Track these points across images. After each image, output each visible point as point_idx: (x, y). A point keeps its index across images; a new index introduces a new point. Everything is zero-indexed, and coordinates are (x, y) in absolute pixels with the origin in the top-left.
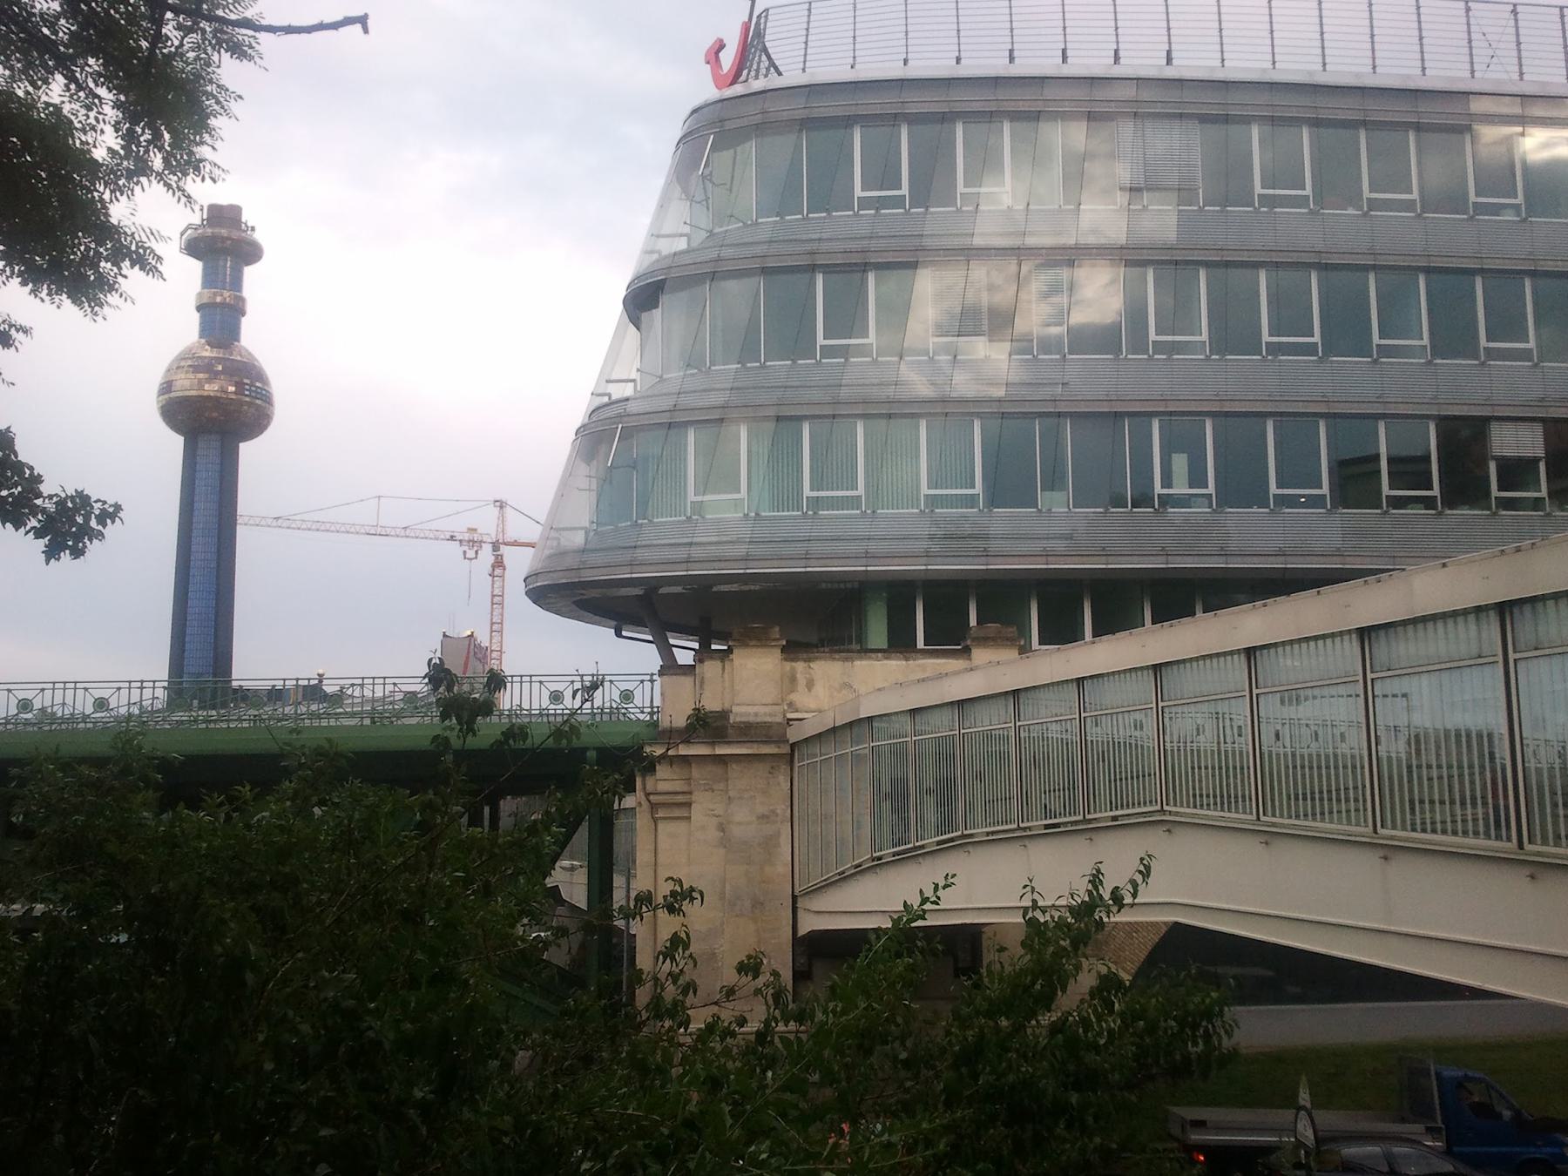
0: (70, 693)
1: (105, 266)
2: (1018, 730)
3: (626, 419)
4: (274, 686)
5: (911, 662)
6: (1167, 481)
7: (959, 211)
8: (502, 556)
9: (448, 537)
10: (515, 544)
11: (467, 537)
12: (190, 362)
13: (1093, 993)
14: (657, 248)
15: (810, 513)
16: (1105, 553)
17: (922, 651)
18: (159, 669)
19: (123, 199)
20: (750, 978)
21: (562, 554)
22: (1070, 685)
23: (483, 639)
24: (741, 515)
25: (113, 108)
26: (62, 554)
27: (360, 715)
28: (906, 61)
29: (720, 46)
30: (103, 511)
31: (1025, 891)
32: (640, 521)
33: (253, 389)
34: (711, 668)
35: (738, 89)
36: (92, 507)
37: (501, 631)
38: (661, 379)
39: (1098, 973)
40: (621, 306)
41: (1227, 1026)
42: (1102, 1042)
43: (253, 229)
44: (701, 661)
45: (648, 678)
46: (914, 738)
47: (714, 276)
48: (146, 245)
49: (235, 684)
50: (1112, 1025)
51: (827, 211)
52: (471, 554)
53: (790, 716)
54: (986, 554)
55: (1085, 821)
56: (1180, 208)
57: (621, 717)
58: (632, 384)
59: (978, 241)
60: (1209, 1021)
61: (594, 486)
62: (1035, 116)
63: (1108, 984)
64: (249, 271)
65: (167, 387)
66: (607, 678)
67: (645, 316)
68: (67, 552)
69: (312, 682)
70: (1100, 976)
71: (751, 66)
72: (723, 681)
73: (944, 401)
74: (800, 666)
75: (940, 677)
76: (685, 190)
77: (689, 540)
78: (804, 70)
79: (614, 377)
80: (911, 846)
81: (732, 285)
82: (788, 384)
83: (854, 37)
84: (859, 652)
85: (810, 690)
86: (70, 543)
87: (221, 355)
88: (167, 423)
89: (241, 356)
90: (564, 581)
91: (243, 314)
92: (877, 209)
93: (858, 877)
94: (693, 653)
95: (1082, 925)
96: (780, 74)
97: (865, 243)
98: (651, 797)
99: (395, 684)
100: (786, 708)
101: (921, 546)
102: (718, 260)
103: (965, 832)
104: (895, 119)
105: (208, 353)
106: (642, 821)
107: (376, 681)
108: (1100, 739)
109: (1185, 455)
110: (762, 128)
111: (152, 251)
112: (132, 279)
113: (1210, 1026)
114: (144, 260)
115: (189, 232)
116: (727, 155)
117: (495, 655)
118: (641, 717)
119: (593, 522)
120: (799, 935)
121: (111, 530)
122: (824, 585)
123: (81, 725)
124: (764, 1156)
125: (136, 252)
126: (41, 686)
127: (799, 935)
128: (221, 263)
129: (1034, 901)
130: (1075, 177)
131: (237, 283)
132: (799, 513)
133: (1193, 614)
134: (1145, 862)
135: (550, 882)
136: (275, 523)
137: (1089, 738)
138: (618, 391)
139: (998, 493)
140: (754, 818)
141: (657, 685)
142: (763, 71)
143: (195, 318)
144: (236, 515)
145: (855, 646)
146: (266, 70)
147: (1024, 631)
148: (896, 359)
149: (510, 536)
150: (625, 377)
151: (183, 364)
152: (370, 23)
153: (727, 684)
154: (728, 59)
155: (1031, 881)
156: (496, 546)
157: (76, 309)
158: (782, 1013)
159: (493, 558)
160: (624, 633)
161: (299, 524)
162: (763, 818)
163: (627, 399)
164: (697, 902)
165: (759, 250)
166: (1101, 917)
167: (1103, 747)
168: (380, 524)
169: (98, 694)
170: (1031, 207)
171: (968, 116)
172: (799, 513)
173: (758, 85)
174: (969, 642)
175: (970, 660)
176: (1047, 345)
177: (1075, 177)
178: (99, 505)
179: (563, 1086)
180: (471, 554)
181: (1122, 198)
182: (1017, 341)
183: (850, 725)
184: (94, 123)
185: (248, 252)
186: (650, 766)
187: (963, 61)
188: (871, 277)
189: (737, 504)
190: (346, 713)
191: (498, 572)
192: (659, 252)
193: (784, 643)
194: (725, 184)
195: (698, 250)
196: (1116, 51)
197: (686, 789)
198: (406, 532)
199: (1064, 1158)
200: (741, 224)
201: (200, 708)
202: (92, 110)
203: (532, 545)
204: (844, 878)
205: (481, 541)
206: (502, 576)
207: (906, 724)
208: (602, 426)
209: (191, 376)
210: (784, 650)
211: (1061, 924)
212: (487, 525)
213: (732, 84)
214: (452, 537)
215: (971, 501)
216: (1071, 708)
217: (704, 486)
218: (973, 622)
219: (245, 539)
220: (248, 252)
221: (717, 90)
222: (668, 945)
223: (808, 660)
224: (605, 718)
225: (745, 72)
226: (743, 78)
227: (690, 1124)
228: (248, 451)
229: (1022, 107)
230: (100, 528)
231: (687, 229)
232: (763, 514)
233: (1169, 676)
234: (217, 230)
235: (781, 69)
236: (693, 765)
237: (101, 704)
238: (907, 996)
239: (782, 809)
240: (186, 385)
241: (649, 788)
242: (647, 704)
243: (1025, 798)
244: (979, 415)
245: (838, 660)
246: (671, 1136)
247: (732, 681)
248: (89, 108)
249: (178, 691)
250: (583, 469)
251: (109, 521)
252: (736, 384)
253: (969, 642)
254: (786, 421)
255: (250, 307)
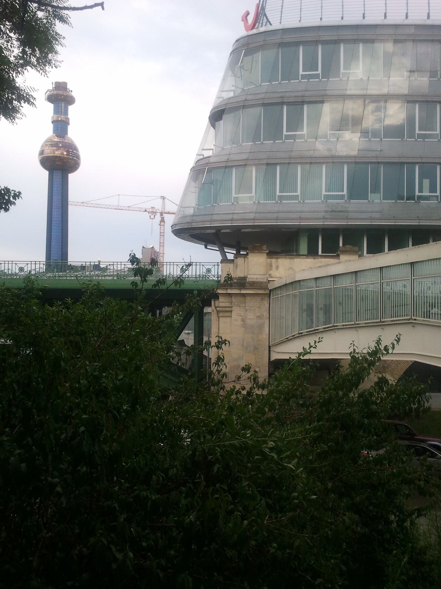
0: (10, 265)
1: (15, 103)
2: (356, 286)
3: (209, 165)
4: (82, 264)
5: (316, 260)
6: (421, 191)
7: (341, 80)
8: (164, 218)
9: (144, 210)
10: (169, 213)
11: (151, 210)
12: (50, 143)
13: (377, 384)
14: (222, 96)
15: (279, 201)
16: (394, 218)
17: (320, 256)
18: (42, 258)
19: (20, 76)
20: (246, 372)
21: (185, 217)
22: (377, 270)
23: (157, 249)
24: (253, 202)
25: (16, 41)
26: (1, 210)
27: (113, 276)
28: (321, 19)
29: (248, 14)
30: (15, 194)
31: (351, 345)
32: (214, 204)
33: (73, 153)
34: (240, 260)
35: (254, 31)
36: (11, 193)
37: (163, 246)
38: (223, 149)
39: (378, 377)
40: (208, 120)
41: (427, 398)
42: (378, 402)
43: (71, 91)
44: (236, 258)
45: (217, 264)
46: (316, 289)
47: (244, 107)
48: (30, 94)
49: (69, 263)
50: (383, 396)
51: (288, 80)
52: (152, 217)
53: (269, 279)
54: (347, 218)
55: (381, 322)
56: (430, 79)
57: (207, 278)
58: (212, 151)
59: (348, 92)
60: (420, 396)
61: (197, 191)
62: (372, 41)
63: (383, 381)
64: (70, 108)
65: (42, 153)
66: (201, 264)
67: (217, 123)
68: (3, 209)
69: (96, 263)
70: (379, 378)
71: (260, 21)
72: (245, 266)
73: (333, 157)
74: (274, 261)
75: (327, 265)
76: (233, 72)
77: (232, 212)
78: (280, 23)
79: (205, 148)
80: (314, 329)
81: (251, 111)
82: (272, 150)
83: (301, 9)
84: (296, 255)
85: (277, 270)
86: (4, 206)
87: (61, 140)
88: (41, 165)
89: (68, 140)
90: (186, 227)
91: (69, 124)
92: (308, 79)
93: (293, 340)
94: (234, 255)
95: (372, 359)
96: (271, 25)
97: (303, 93)
98: (217, 308)
99: (125, 265)
100: (268, 276)
101: (321, 215)
102: (246, 100)
103: (334, 325)
104: (316, 43)
105: (56, 139)
106: (214, 317)
107: (118, 263)
108: (388, 291)
109: (429, 180)
110: (262, 47)
111: (32, 96)
112: (25, 108)
113: (420, 398)
114: (27, 99)
115: (48, 92)
116: (250, 58)
117: (161, 255)
118: (214, 278)
119: (197, 205)
120: (271, 360)
121: (18, 201)
122: (283, 230)
123: (15, 277)
124: (248, 435)
125: (26, 97)
126: (27, 263)
127: (271, 360)
128: (60, 104)
129: (354, 350)
130: (388, 64)
131: (66, 113)
132: (275, 202)
133: (428, 242)
134: (398, 337)
135: (180, 338)
136: (82, 205)
137: (384, 291)
138: (207, 154)
139: (352, 195)
140: (255, 317)
141: (220, 267)
142: (264, 24)
143: (51, 126)
144: (68, 201)
145: (295, 253)
146: (73, 27)
147: (361, 249)
148: (315, 140)
149: (167, 210)
150: (209, 148)
151: (47, 143)
152: (104, 5)
153: (246, 267)
154: (251, 19)
155: (353, 342)
156: (161, 214)
157: (6, 120)
158: (256, 385)
159: (161, 218)
160: (208, 247)
161: (90, 205)
162: (259, 317)
163: (210, 157)
164: (228, 345)
165: (261, 96)
166: (380, 356)
167: (389, 294)
168: (120, 205)
169: (20, 266)
170: (370, 78)
171: (346, 41)
172: (275, 202)
173: (262, 29)
174: (339, 253)
175: (339, 259)
176: (375, 134)
177: (388, 64)
178: (13, 192)
179: (178, 408)
180: (152, 217)
181: (406, 74)
182: (363, 133)
183: (292, 283)
184: (10, 48)
185: (69, 100)
186: (216, 297)
187: (344, 18)
188: (305, 107)
189: (251, 198)
190: (108, 275)
191: (162, 224)
192: (223, 97)
193: (268, 251)
194: (249, 70)
195: (238, 96)
196: (407, 14)
197: (230, 306)
198: (129, 208)
199: (362, 443)
200: (255, 86)
201: (57, 272)
202: (9, 42)
203: (174, 214)
204: (288, 340)
205: (156, 212)
206: (164, 225)
207: (313, 284)
208: (201, 167)
209: (51, 148)
210: (267, 254)
211: (365, 359)
212: (158, 205)
213: (252, 29)
214: (145, 210)
215: (342, 197)
216: (377, 278)
217: (238, 191)
218: (341, 245)
219: (71, 210)
220: (69, 100)
221: (246, 32)
222: (216, 359)
223: (277, 258)
224: (201, 279)
225: (257, 24)
226: (256, 27)
227: (222, 423)
228: (71, 177)
229: (367, 37)
230: (14, 200)
231: (233, 88)
232: (261, 202)
233: (416, 267)
234: (58, 92)
235: (271, 22)
236: (233, 297)
237: (21, 269)
238: (305, 382)
239: (266, 314)
240: (49, 152)
241: (216, 305)
242: (216, 274)
243: (358, 313)
244: (347, 163)
245: (288, 258)
246: (214, 426)
247: (248, 266)
248: (8, 42)
249: (48, 265)
250: (193, 184)
251: (17, 198)
252: (252, 151)
253: (339, 253)
254: (271, 165)
255: (71, 122)
